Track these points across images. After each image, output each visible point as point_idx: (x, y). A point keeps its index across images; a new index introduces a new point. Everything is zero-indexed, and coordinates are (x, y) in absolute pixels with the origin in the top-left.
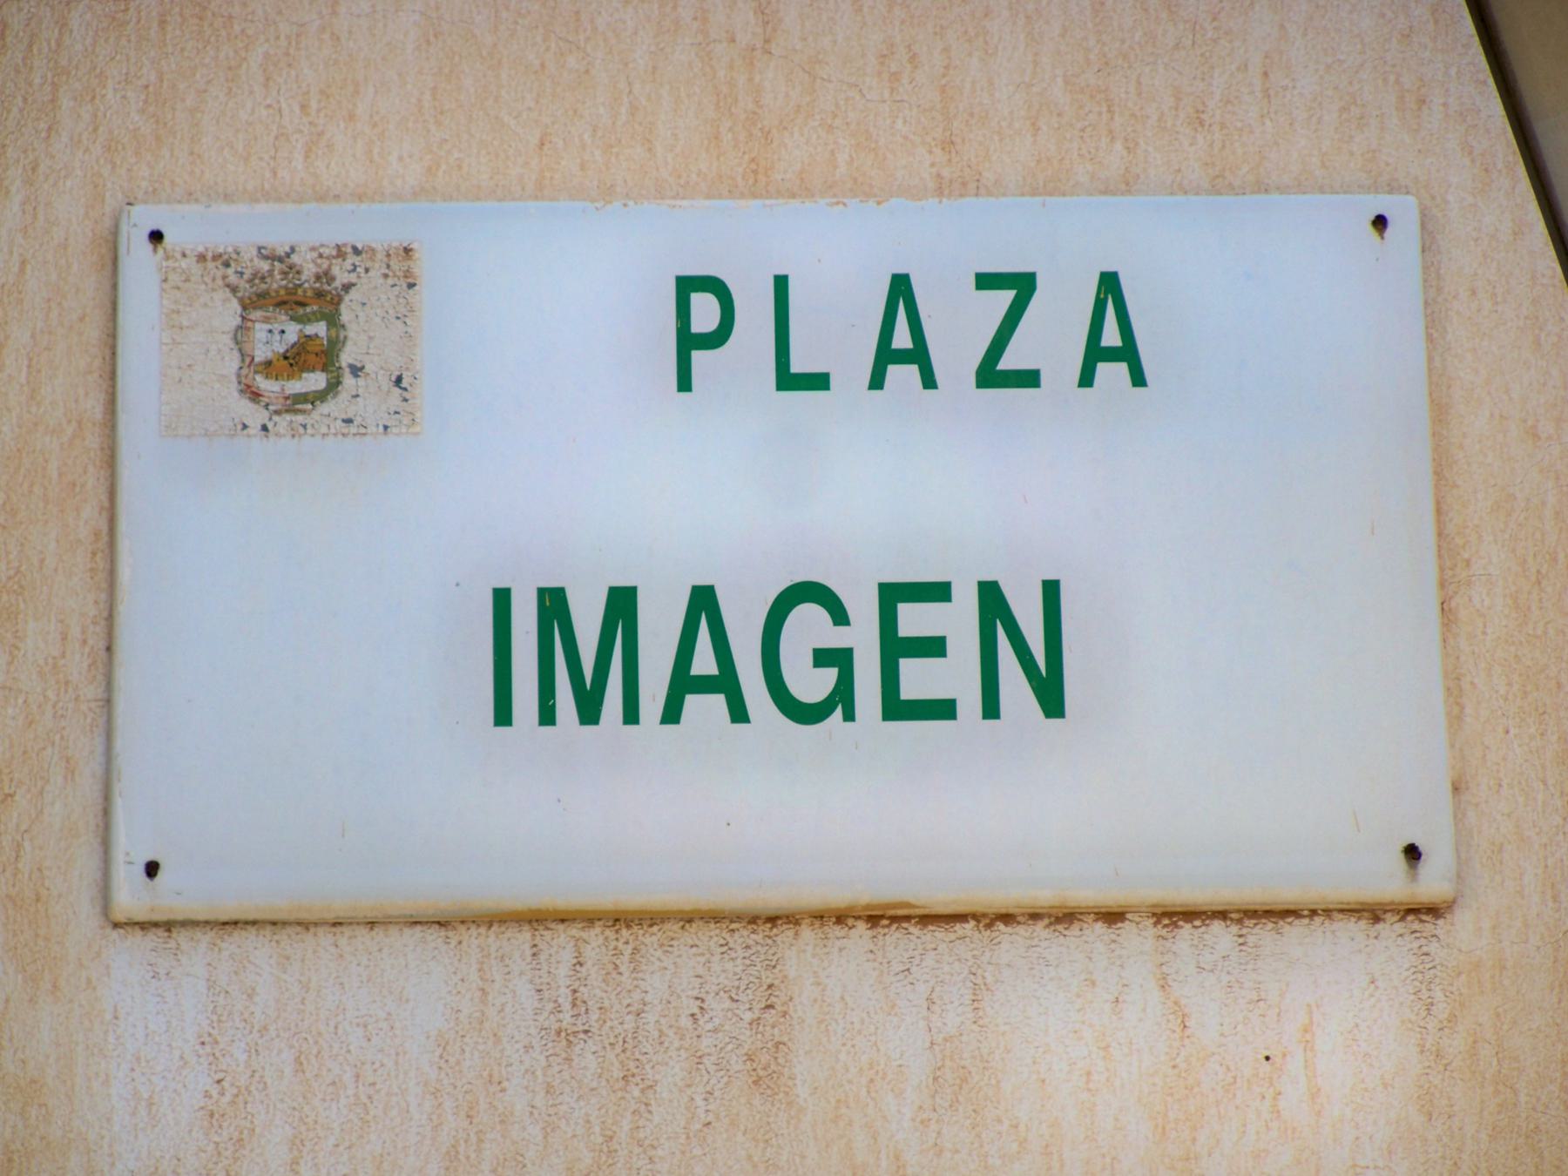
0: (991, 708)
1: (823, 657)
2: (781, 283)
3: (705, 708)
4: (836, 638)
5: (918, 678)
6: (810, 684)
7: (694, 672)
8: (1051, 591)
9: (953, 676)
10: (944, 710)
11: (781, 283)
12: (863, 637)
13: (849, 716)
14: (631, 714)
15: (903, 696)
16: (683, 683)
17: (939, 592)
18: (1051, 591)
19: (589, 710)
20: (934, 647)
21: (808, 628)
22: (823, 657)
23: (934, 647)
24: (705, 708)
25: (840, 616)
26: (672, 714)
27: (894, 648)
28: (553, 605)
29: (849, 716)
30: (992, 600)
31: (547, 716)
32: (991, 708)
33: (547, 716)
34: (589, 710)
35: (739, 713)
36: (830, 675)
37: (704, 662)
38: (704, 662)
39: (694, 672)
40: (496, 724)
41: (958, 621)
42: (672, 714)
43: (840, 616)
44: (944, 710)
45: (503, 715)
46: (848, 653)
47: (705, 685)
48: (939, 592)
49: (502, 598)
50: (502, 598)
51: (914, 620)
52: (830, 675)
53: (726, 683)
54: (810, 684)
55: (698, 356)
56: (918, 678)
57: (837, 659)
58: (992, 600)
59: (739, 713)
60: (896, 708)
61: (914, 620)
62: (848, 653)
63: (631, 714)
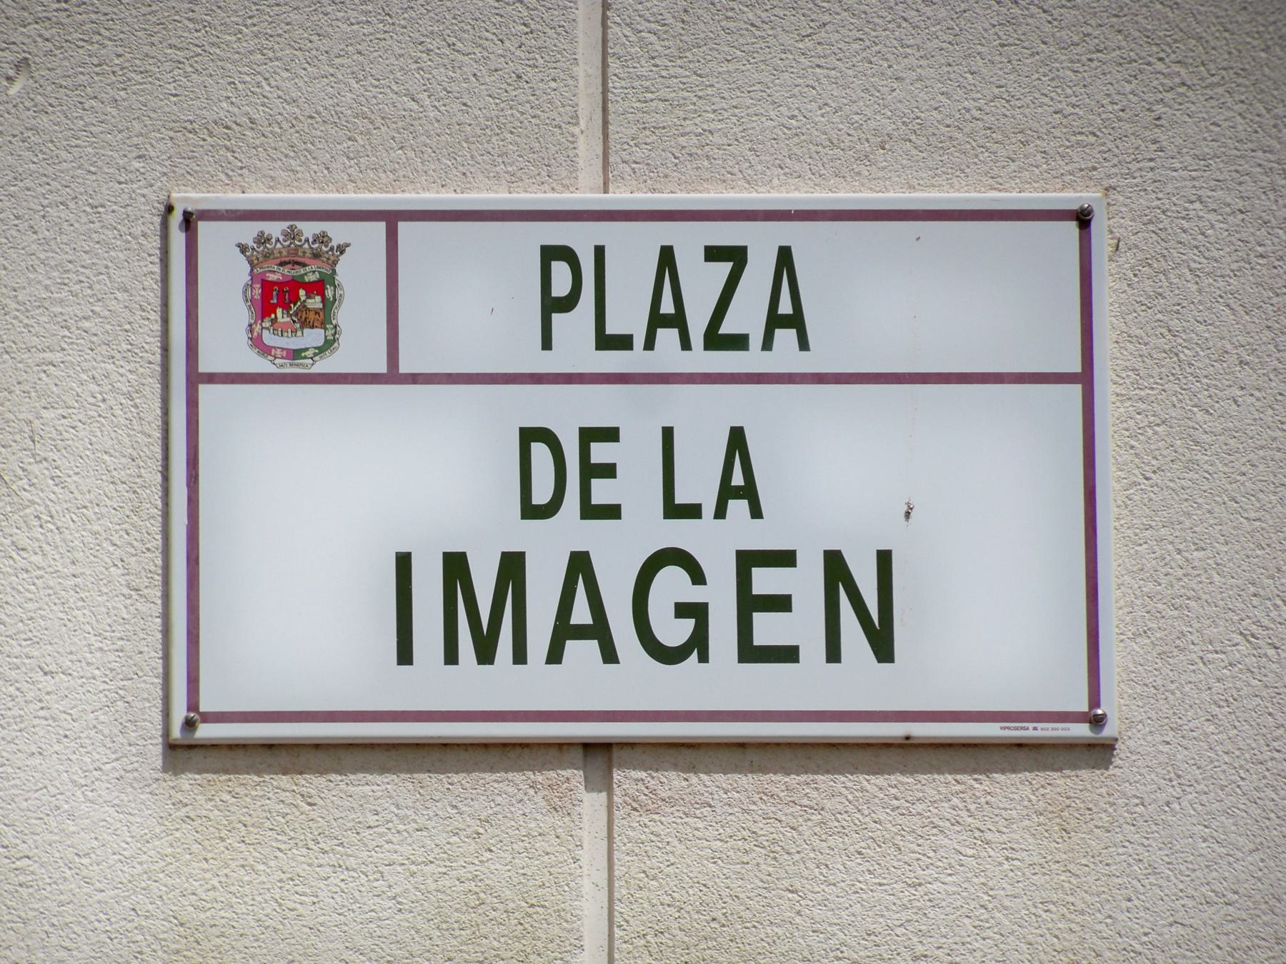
0: (833, 654)
1: (683, 610)
2: (668, 434)
3: (582, 652)
4: (694, 594)
5: (767, 629)
6: (674, 632)
7: (572, 622)
8: (884, 559)
9: (801, 626)
10: (788, 654)
11: (668, 434)
12: (720, 597)
13: (704, 658)
14: (520, 656)
15: (756, 643)
16: (564, 631)
17: (785, 559)
18: (884, 559)
19: (486, 654)
20: (781, 603)
21: (672, 585)
22: (683, 610)
23: (781, 603)
24: (582, 652)
25: (698, 577)
26: (555, 656)
27: (749, 604)
28: (456, 567)
29: (704, 658)
30: (835, 567)
31: (451, 656)
32: (833, 654)
33: (451, 656)
34: (486, 654)
35: (610, 655)
36: (689, 625)
37: (581, 614)
38: (581, 614)
39: (572, 622)
40: (790, 610)
41: (805, 583)
42: (555, 656)
43: (698, 577)
44: (788, 654)
45: (405, 655)
46: (704, 607)
47: (581, 633)
48: (785, 559)
49: (404, 563)
50: (404, 563)
51: (765, 581)
52: (689, 625)
53: (599, 630)
54: (674, 632)
55: (556, 318)
56: (767, 629)
57: (695, 612)
58: (835, 567)
59: (610, 655)
60: (750, 652)
61: (765, 581)
62: (704, 607)
63: (520, 656)
